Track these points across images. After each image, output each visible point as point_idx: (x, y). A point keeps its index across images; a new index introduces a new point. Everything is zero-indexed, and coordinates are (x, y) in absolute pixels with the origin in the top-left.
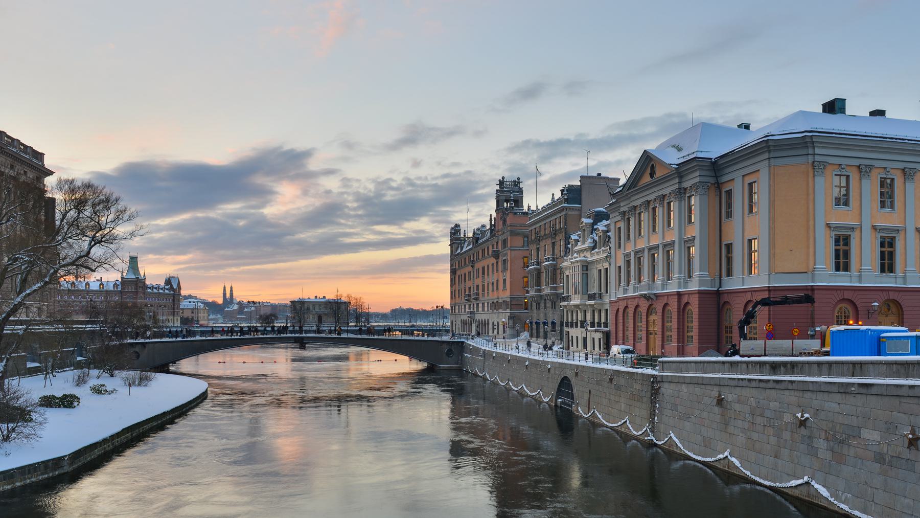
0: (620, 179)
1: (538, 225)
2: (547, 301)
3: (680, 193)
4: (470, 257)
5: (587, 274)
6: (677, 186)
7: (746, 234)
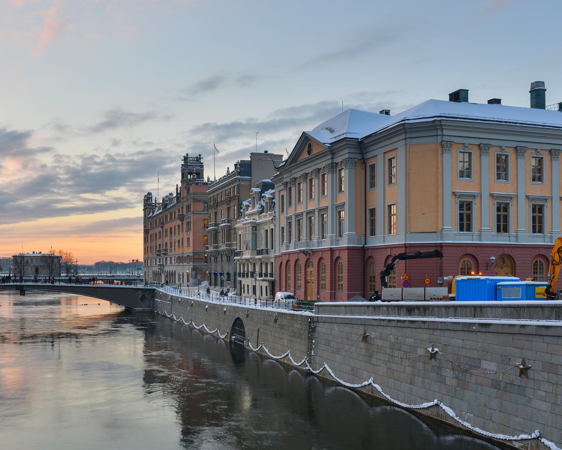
0: (283, 155)
1: (216, 194)
2: (223, 256)
3: (332, 167)
4: (160, 220)
5: (256, 233)
6: (330, 161)
7: (386, 200)
